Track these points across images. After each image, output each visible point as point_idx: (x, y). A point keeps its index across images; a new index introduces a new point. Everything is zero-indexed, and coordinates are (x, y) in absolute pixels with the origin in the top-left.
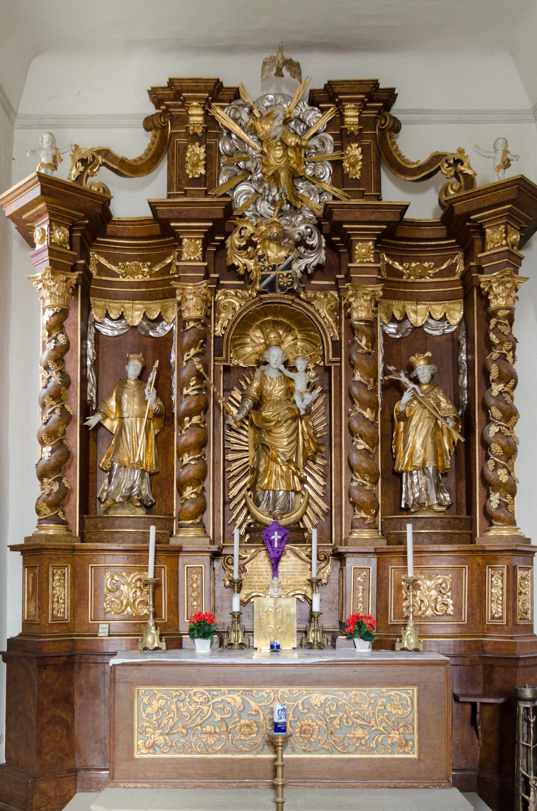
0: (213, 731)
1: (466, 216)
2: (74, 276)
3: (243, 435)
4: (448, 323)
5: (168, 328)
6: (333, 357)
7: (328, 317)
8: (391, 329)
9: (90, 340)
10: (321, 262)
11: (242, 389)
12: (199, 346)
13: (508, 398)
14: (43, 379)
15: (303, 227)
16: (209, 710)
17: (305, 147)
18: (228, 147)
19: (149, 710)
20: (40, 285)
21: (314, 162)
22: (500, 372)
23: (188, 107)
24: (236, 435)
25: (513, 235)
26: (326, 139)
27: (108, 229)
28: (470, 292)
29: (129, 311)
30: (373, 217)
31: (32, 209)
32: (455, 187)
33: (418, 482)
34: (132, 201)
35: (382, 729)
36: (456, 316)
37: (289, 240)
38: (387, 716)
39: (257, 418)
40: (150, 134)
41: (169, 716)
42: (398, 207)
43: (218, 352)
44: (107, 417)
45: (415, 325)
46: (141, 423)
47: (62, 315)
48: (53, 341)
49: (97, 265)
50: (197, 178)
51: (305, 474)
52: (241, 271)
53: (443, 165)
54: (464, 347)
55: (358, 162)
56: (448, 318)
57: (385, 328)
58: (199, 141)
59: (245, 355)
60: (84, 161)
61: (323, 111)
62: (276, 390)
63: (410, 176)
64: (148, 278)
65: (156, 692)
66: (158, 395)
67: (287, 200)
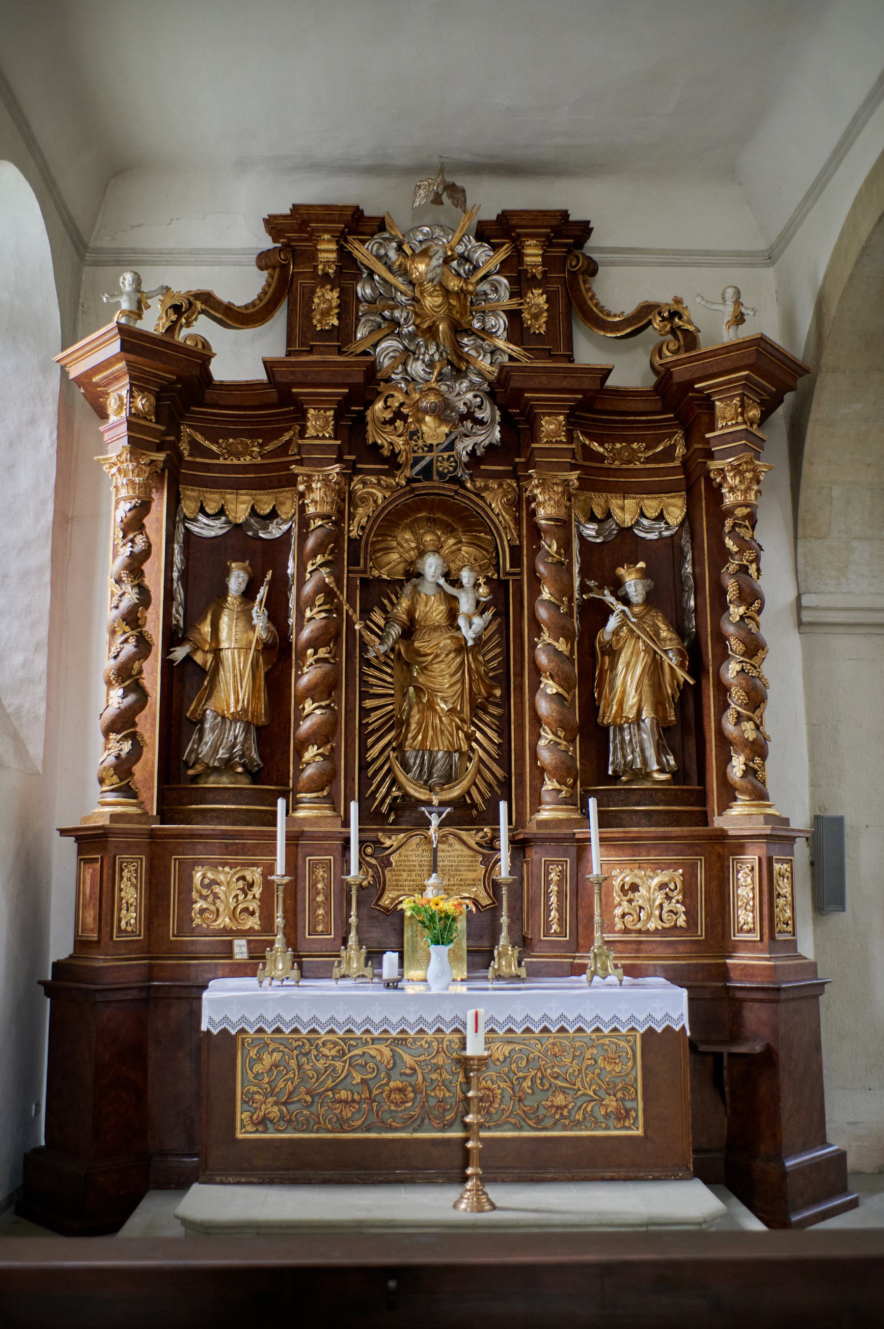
0: (350, 1099)
1: (688, 385)
2: (161, 457)
3: (386, 673)
4: (666, 523)
5: (285, 527)
6: (511, 567)
7: (504, 513)
8: (590, 530)
9: (178, 543)
10: (494, 441)
11: (384, 610)
12: (328, 552)
13: (752, 625)
14: (112, 596)
15: (470, 395)
16: (344, 1067)
17: (471, 293)
18: (368, 291)
19: (258, 1068)
20: (114, 470)
21: (484, 312)
22: (740, 590)
23: (317, 240)
24: (377, 674)
25: (751, 410)
26: (499, 282)
27: (207, 396)
28: (698, 487)
29: (232, 503)
30: (564, 384)
31: (107, 369)
32: (672, 347)
33: (631, 740)
34: (240, 358)
35: (591, 1093)
36: (676, 513)
37: (452, 412)
38: (598, 1075)
39: (407, 651)
40: (265, 273)
41: (287, 1076)
42: (598, 372)
43: (354, 560)
44: (198, 648)
45: (622, 526)
46: (247, 654)
47: (142, 508)
48: (130, 544)
49: (190, 443)
50: (327, 331)
51: (473, 728)
52: (386, 452)
53: (655, 318)
54: (689, 557)
55: (543, 313)
56: (666, 516)
57: (581, 528)
58: (331, 284)
59: (390, 563)
60: (177, 308)
61: (495, 247)
62: (436, 611)
63: (611, 332)
64: (259, 460)
65: (269, 1042)
66: (270, 618)
67: (448, 360)
